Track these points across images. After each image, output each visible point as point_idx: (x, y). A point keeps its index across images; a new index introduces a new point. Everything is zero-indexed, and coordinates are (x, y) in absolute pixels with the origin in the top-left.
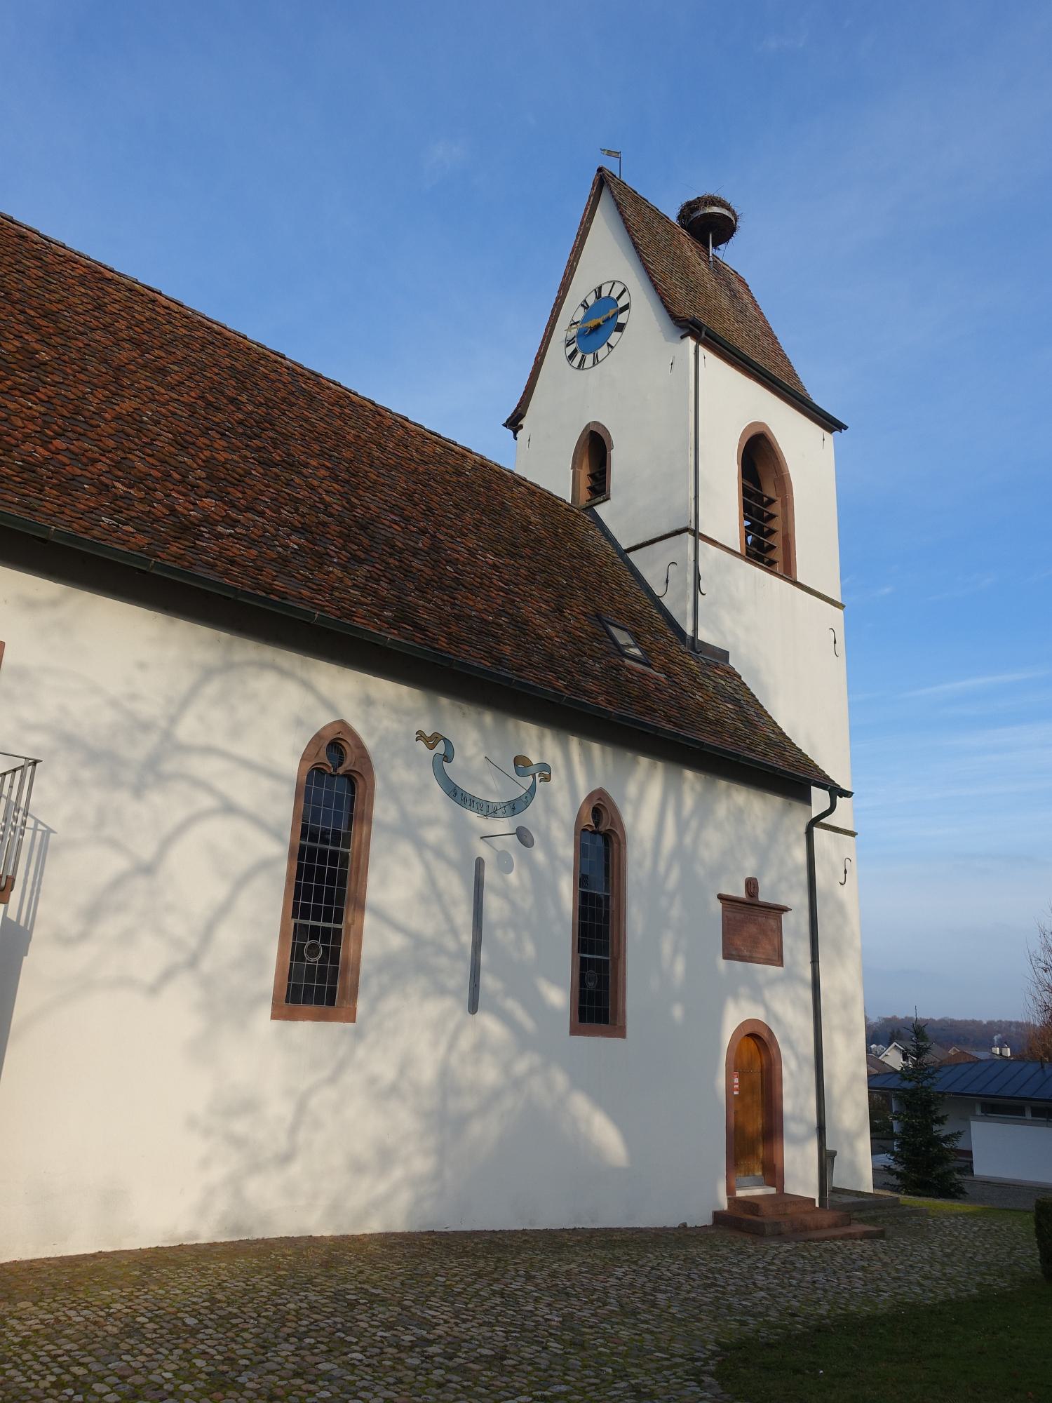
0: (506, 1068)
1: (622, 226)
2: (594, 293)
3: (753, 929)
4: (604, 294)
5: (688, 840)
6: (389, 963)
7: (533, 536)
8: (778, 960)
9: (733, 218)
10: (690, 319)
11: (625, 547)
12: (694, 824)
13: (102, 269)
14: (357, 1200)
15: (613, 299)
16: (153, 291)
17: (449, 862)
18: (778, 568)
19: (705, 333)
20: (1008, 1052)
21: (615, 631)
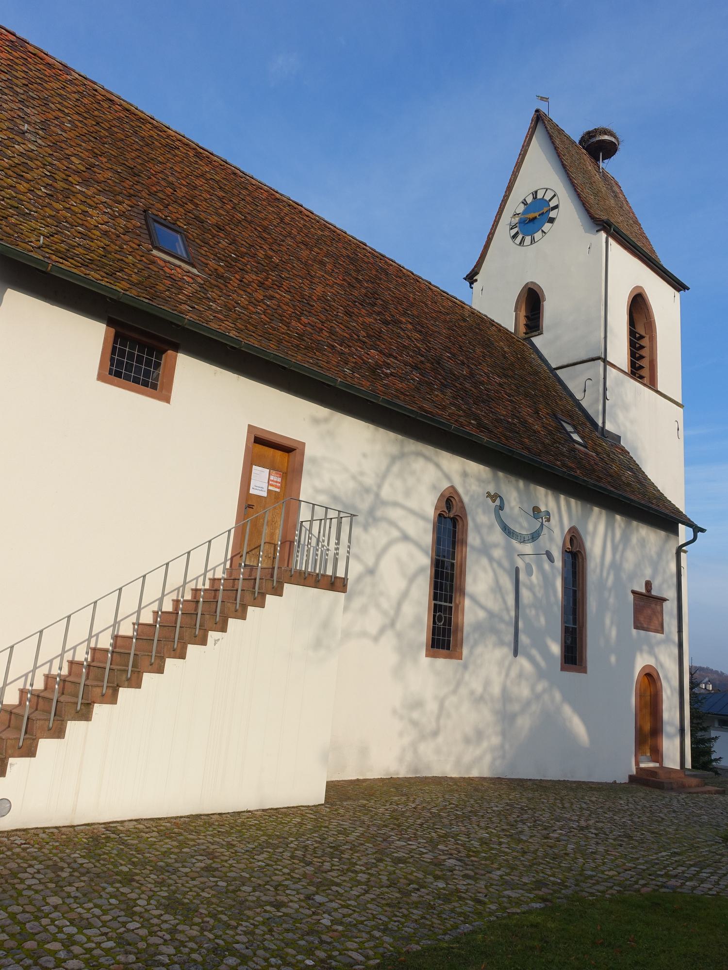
0: (533, 689)
1: (554, 152)
2: (531, 195)
3: (649, 612)
4: (540, 196)
5: (618, 557)
6: (478, 627)
7: (509, 362)
8: (660, 629)
9: (617, 143)
10: (605, 221)
11: (554, 366)
12: (621, 547)
13: (274, 193)
14: (467, 759)
15: (546, 200)
17: (504, 569)
18: (646, 381)
19: (614, 230)
20: (710, 687)
21: (565, 425)
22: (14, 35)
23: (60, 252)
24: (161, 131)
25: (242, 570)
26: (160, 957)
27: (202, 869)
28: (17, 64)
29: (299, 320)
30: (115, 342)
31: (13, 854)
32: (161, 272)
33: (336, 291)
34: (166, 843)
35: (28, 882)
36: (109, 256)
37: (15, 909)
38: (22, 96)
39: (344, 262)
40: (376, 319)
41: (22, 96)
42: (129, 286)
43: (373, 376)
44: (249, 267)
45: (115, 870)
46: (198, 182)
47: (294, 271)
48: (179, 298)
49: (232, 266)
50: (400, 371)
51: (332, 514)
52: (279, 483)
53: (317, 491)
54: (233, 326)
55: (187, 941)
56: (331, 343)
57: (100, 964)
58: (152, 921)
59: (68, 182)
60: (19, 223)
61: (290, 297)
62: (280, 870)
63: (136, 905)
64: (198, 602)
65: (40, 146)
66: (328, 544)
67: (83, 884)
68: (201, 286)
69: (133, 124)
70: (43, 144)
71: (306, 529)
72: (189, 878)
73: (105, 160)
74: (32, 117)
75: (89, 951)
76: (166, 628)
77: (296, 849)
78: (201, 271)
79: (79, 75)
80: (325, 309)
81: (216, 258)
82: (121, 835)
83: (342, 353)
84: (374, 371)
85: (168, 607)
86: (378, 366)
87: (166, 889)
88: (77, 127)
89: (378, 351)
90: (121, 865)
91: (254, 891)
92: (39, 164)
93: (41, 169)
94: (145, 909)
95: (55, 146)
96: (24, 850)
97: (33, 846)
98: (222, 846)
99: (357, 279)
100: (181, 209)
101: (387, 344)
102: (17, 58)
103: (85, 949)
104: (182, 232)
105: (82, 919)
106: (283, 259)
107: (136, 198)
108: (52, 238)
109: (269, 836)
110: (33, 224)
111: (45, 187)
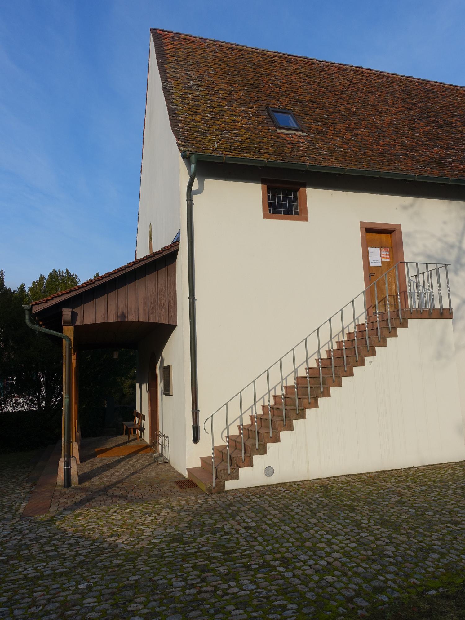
16: (359, 68)
22: (172, 32)
23: (227, 148)
24: (263, 55)
25: (378, 315)
26: (387, 552)
27: (396, 502)
28: (178, 49)
29: (378, 144)
30: (268, 193)
31: (282, 496)
32: (285, 142)
33: (399, 116)
34: (368, 488)
35: (296, 511)
36: (254, 142)
37: (294, 525)
38: (185, 66)
39: (400, 95)
40: (432, 127)
41: (185, 66)
42: (269, 156)
43: (440, 166)
44: (337, 120)
45: (343, 504)
46: (293, 78)
47: (367, 113)
48: (300, 154)
49: (326, 123)
50: (460, 157)
51: (431, 267)
52: (388, 255)
53: (416, 255)
54: (336, 161)
55: (401, 544)
56: (404, 152)
57: (351, 555)
58: (374, 532)
59: (220, 106)
60: (202, 139)
61: (368, 131)
62: (449, 502)
63: (362, 523)
64: (342, 349)
65: (201, 91)
66: (432, 289)
67: (326, 512)
68: (310, 142)
69: (247, 57)
70: (202, 89)
71: (413, 282)
72: (389, 508)
73: (237, 85)
74: (193, 76)
75: (342, 548)
76: (337, 359)
77: (456, 489)
78: (308, 133)
79: (211, 41)
80: (394, 131)
81: (315, 121)
82: (339, 484)
83: (413, 157)
84: (439, 162)
85: (324, 355)
86: (441, 158)
87: (377, 514)
88: (217, 72)
89: (439, 148)
90: (345, 501)
91: (435, 514)
92: (203, 101)
93: (205, 104)
94: (369, 526)
95: (209, 88)
96: (287, 494)
97: (291, 492)
98: (404, 489)
99: (412, 103)
100: (287, 99)
101: (445, 141)
102: (177, 45)
103: (340, 547)
104: (291, 112)
105: (333, 531)
106: (358, 107)
107: (260, 101)
108: (221, 142)
109: (434, 482)
110: (209, 137)
111: (210, 114)
